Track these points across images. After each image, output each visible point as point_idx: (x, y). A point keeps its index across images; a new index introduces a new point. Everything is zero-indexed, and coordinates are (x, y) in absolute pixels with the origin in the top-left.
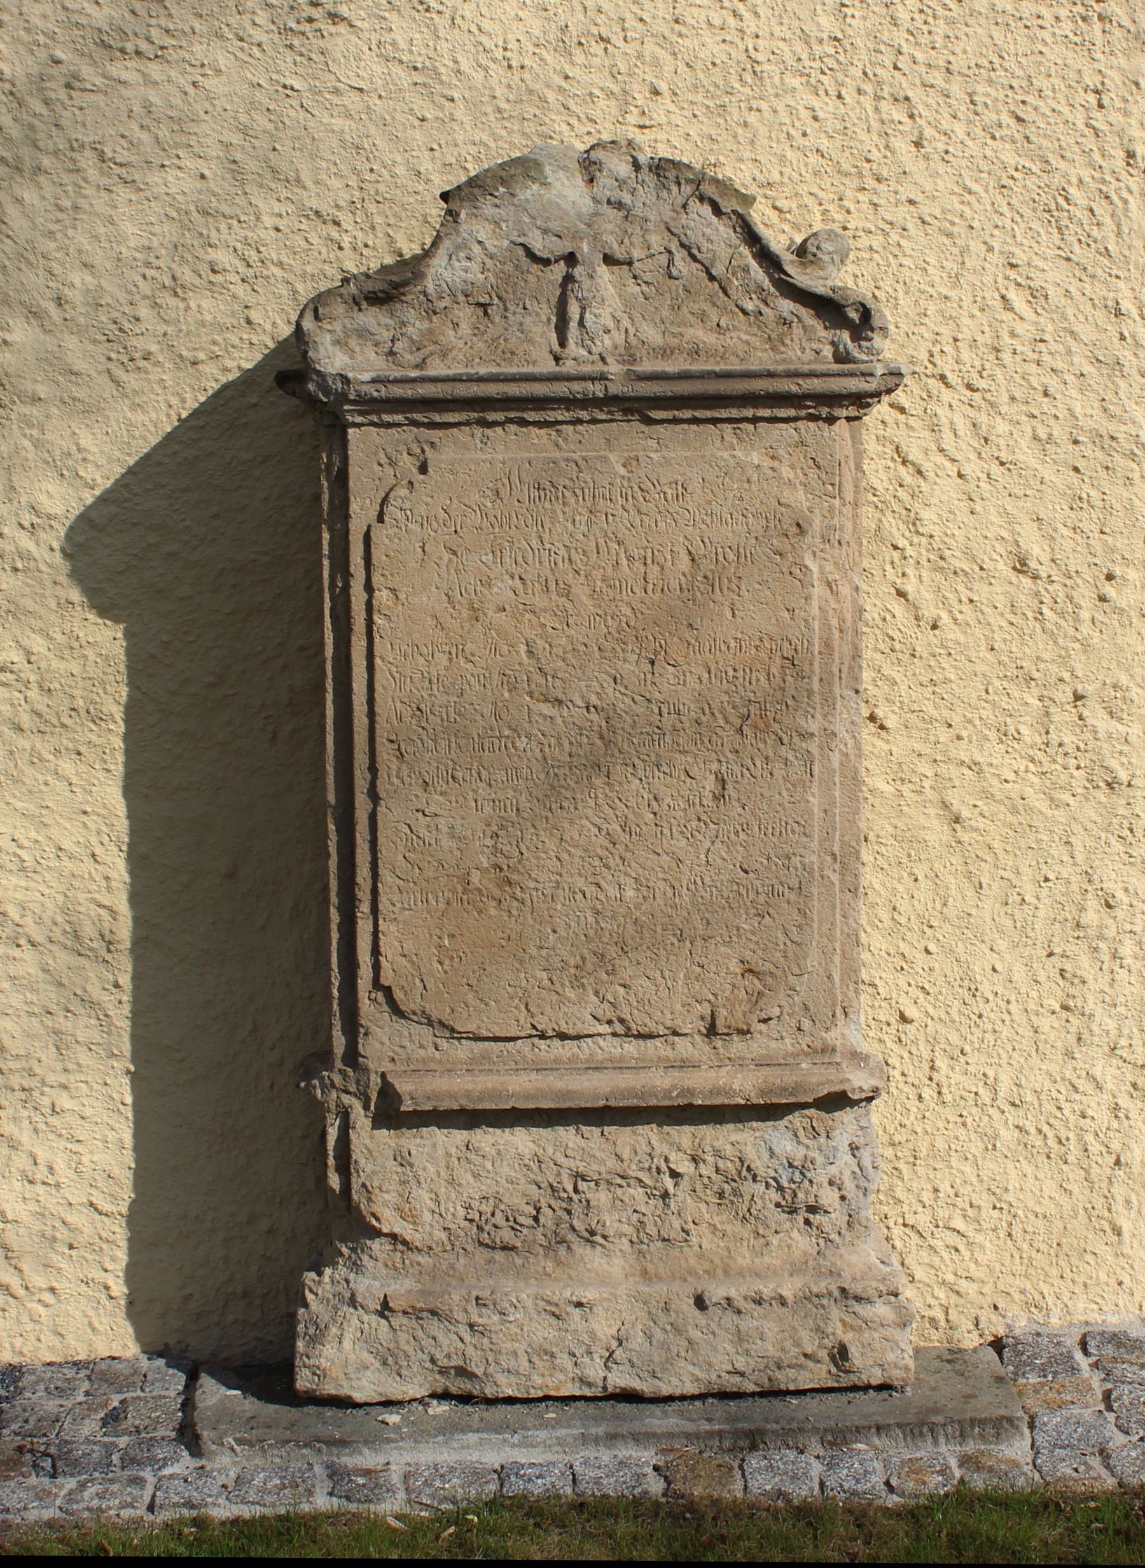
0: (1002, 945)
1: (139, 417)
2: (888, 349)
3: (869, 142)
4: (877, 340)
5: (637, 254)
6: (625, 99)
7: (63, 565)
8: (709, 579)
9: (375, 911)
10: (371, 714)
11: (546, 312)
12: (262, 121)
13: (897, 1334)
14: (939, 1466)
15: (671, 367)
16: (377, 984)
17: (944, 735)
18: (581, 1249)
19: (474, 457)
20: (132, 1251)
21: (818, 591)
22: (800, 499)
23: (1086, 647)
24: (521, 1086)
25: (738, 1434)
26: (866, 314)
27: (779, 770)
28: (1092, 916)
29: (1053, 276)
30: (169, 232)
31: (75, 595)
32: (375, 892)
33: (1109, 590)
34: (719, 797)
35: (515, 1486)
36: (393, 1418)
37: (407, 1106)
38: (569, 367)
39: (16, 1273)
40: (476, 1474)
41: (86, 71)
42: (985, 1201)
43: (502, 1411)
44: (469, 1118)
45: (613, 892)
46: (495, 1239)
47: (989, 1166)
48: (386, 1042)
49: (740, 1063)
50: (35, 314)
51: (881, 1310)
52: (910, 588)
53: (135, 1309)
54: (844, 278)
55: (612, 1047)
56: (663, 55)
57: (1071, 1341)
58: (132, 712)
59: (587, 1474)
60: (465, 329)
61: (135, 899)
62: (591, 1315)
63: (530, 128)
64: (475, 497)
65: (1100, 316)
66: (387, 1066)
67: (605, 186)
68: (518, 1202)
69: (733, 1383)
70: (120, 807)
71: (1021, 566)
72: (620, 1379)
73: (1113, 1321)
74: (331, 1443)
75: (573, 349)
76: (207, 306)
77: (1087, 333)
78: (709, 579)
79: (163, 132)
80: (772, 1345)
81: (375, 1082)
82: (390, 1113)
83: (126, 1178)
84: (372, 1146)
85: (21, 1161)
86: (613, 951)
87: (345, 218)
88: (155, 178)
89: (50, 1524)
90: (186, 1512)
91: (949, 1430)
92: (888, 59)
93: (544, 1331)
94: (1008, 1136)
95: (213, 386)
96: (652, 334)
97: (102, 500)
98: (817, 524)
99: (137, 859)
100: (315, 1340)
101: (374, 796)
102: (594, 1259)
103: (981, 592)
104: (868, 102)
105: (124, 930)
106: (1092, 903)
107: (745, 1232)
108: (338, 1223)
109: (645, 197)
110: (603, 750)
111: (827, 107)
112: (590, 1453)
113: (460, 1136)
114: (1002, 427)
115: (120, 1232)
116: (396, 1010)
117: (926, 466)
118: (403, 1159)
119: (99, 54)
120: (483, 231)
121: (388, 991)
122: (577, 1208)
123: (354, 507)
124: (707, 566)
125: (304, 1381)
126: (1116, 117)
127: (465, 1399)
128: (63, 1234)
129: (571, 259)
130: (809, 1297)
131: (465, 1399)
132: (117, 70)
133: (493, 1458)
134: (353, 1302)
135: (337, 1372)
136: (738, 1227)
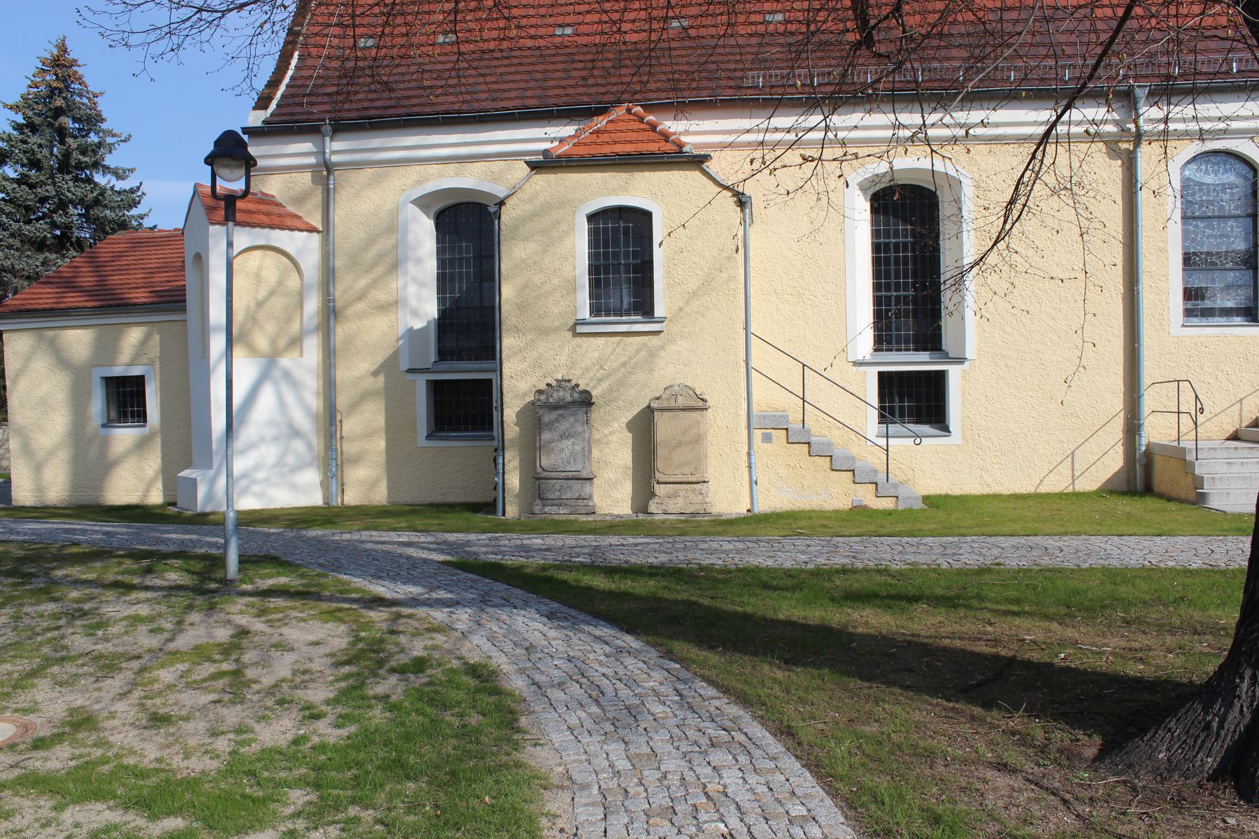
19: (666, 414)
48: (657, 475)
54: (705, 397)
82: (658, 483)
90: (73, 763)
108: (653, 495)
110: (679, 444)
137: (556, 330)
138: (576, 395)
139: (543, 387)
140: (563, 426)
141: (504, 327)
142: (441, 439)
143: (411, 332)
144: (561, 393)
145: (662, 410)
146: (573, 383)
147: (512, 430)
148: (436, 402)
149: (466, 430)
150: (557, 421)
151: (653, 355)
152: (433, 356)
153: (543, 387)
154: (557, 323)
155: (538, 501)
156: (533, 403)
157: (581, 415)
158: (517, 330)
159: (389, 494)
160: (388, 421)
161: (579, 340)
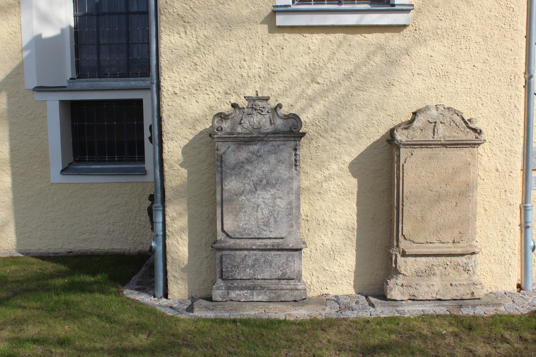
0: (492, 230)
1: (361, 147)
2: (484, 136)
3: (475, 104)
4: (482, 135)
5: (446, 122)
6: (437, 98)
7: (348, 170)
8: (456, 172)
9: (402, 223)
10: (403, 192)
11: (431, 131)
12: (381, 101)
13: (481, 290)
14: (491, 311)
15: (451, 139)
16: (402, 234)
17: (484, 197)
18: (432, 276)
19: (419, 153)
20: (355, 277)
21: (472, 174)
22: (469, 160)
23: (507, 183)
24: (425, 251)
25: (459, 305)
26: (481, 131)
27: (465, 201)
28: (506, 226)
29: (503, 125)
30: (366, 118)
31: (350, 174)
32: (402, 220)
33: (511, 174)
34: (456, 206)
35: (426, 313)
36: (404, 303)
37: (407, 254)
38: (435, 139)
40: (419, 311)
41: (354, 93)
42: (489, 271)
43: (419, 302)
44: (416, 256)
45: (439, 220)
46: (419, 274)
47: (489, 265)
48: (403, 244)
49: (458, 247)
50: (345, 131)
51: (479, 286)
52: (480, 174)
53: (355, 287)
55: (438, 245)
56: (443, 91)
57: (503, 293)
58: (358, 193)
59: (437, 311)
60: (419, 133)
61: (357, 222)
62: (435, 287)
63: (422, 102)
64: (420, 159)
65: (510, 131)
66: (403, 247)
67: (440, 111)
68: (423, 269)
69: (456, 298)
70: (356, 208)
71: (497, 170)
72: (438, 297)
73: (509, 290)
74: (395, 306)
75: (436, 136)
76: (372, 129)
77: (508, 134)
78: (456, 172)
79: (366, 102)
80: (463, 292)
81: (401, 250)
83: (354, 266)
84: (401, 260)
85: (338, 263)
86: (439, 230)
87: (393, 116)
88: (364, 110)
89: (355, 318)
92: (478, 91)
93: (427, 289)
94: (493, 260)
95: (372, 142)
96: (447, 134)
97: (355, 159)
98: (472, 164)
99: (358, 215)
100: (391, 290)
101: (403, 205)
102: (434, 278)
103: (491, 174)
104: (475, 98)
105: (356, 227)
106: (507, 223)
107: (458, 274)
109: (446, 113)
110: (439, 198)
111: (468, 99)
112: (436, 308)
113: (414, 258)
114: (495, 149)
115: (353, 274)
116: (405, 239)
117: (483, 155)
118: (405, 262)
119: (356, 90)
120: (422, 118)
121: (404, 236)
122: (432, 270)
123: (401, 160)
124: (455, 170)
125: (389, 297)
126: (513, 100)
127: (414, 300)
128: (344, 275)
129: (435, 122)
130: (468, 284)
131: (414, 300)
132: (358, 93)
133: (421, 309)
134: (397, 284)
135: (394, 295)
136: (456, 273)
137: (243, 22)
138: (279, 122)
139: (226, 108)
140: (259, 170)
141: (162, 18)
142: (80, 173)
143: (38, 40)
144: (256, 119)
145: (413, 145)
146: (273, 103)
147: (176, 174)
148: (73, 128)
149: (112, 161)
150: (249, 161)
151: (392, 62)
152: (69, 72)
154: (245, 12)
155: (220, 282)
156: (210, 134)
157: (286, 153)
158: (184, 21)
159: (18, 240)
160: (13, 151)
161: (279, 38)
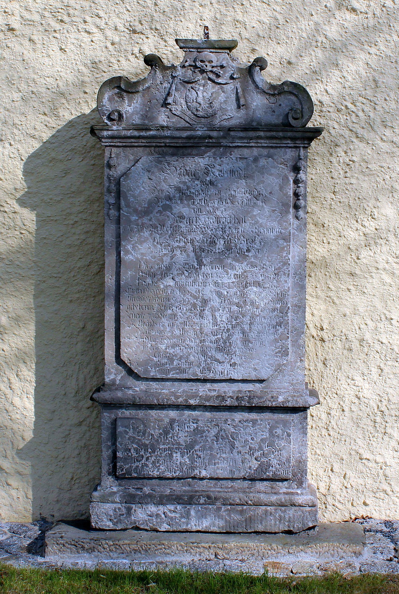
39: (389, 485)
91: (279, 431)
138: (258, 103)
140: (208, 217)
144: (203, 94)
146: (243, 57)
150: (184, 194)
153: (131, 67)
155: (109, 484)
156: (93, 128)
157: (274, 177)
